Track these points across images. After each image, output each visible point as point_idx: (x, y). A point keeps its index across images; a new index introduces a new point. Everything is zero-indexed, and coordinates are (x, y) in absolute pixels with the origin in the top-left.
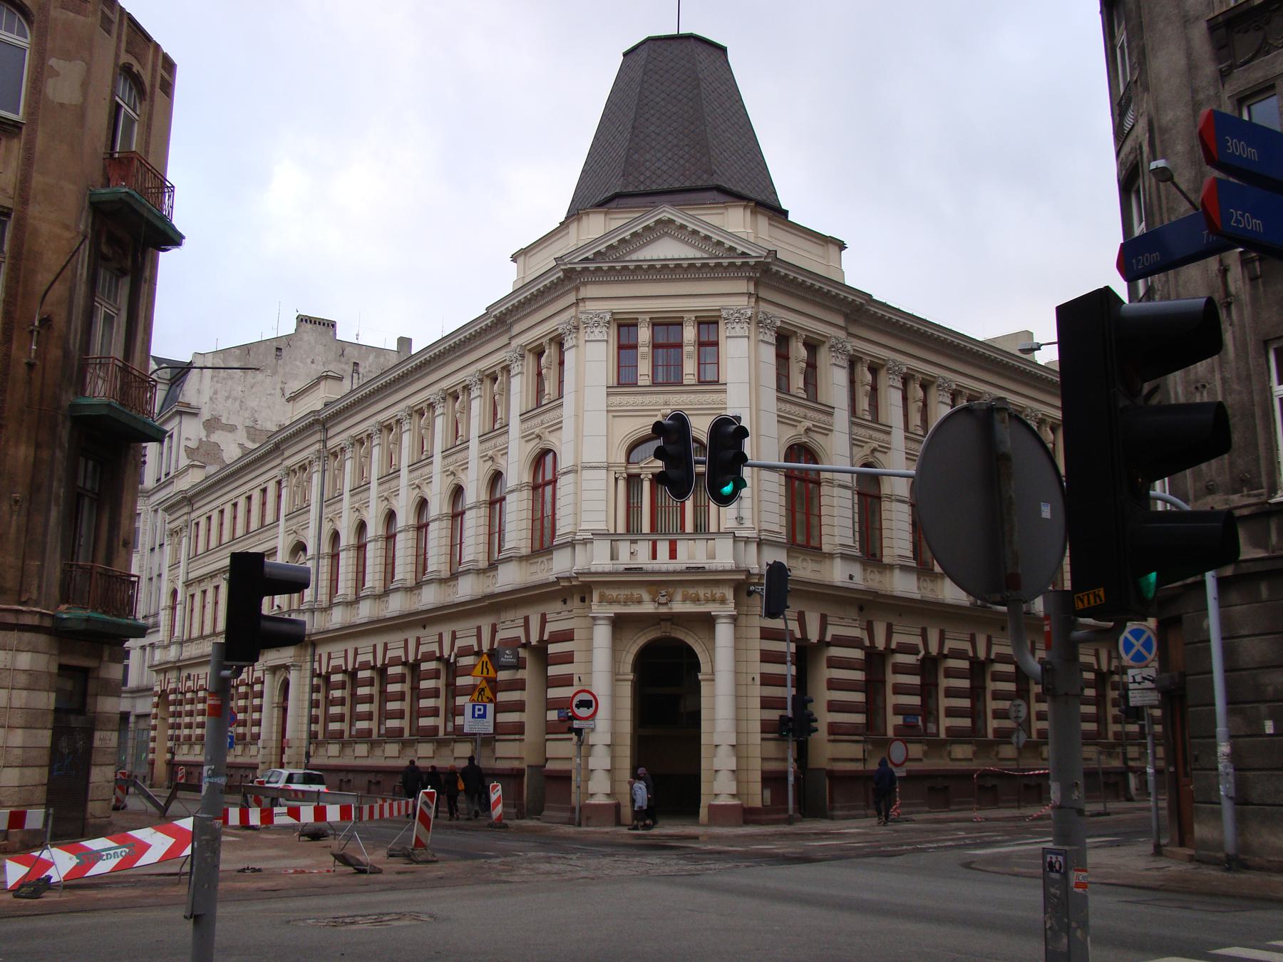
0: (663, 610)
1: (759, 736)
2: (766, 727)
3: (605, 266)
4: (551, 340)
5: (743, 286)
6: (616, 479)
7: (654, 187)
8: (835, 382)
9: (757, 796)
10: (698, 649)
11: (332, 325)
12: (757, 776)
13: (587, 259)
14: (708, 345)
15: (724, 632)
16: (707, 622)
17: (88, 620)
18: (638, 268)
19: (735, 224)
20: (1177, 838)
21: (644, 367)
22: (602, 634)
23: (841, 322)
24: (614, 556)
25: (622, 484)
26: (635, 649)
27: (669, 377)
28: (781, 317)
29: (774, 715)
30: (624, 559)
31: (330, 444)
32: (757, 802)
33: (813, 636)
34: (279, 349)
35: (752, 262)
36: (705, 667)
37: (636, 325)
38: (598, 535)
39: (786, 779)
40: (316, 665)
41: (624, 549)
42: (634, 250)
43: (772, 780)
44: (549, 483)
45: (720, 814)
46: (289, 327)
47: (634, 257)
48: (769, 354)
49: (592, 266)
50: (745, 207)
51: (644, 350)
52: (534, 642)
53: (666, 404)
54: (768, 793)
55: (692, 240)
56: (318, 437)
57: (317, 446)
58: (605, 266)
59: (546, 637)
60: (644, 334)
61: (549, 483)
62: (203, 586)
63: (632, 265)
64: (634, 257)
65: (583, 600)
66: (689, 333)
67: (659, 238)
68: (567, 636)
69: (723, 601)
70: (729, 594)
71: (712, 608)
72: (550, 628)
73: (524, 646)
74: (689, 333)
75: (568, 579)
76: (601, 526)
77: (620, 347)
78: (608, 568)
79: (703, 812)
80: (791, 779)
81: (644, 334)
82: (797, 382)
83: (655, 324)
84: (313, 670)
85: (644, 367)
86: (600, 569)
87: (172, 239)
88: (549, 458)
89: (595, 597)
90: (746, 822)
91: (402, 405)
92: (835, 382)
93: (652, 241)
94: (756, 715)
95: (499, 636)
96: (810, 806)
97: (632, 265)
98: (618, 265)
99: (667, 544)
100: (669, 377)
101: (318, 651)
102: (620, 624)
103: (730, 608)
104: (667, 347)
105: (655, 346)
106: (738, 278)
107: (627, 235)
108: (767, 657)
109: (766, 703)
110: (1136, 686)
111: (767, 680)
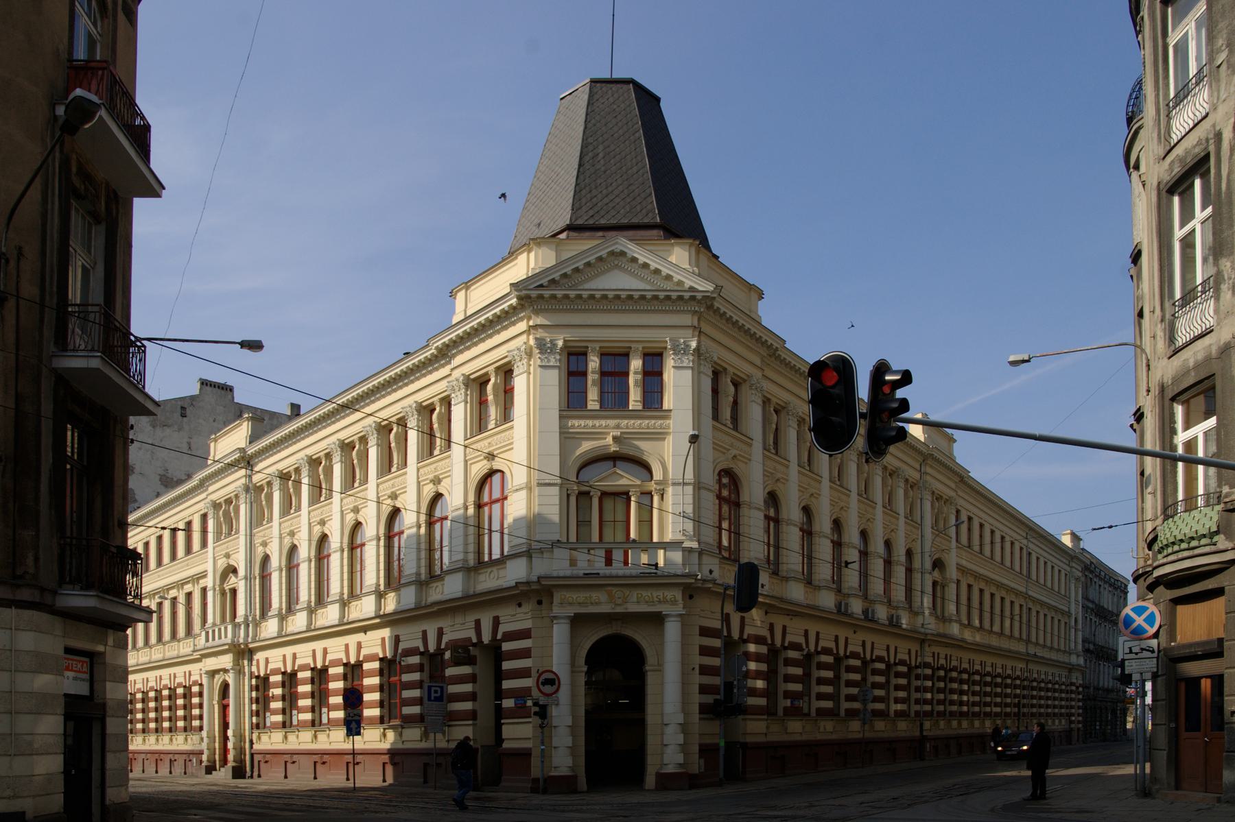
0: (619, 610)
1: (697, 716)
2: (704, 709)
3: (559, 293)
4: (498, 369)
5: (687, 319)
6: (568, 495)
7: (603, 222)
8: (754, 414)
9: (696, 766)
10: (644, 644)
11: (231, 389)
12: (696, 748)
13: (541, 286)
14: (653, 374)
15: (672, 630)
16: (656, 620)
17: (495, 396)
18: (592, 297)
19: (677, 260)
20: (1173, 784)
21: (593, 395)
22: (560, 632)
23: (758, 361)
24: (573, 563)
25: (573, 500)
26: (587, 645)
27: (615, 401)
28: (718, 353)
29: (709, 699)
30: (583, 566)
31: (256, 478)
32: (695, 769)
33: (736, 635)
34: (183, 408)
35: (699, 296)
36: (651, 659)
37: (585, 354)
38: (556, 544)
39: (718, 750)
40: (254, 669)
41: (582, 557)
42: (587, 281)
43: (707, 751)
44: (497, 501)
45: (666, 781)
46: (195, 390)
47: (587, 286)
48: (707, 384)
49: (547, 293)
50: (691, 245)
51: (592, 377)
52: (486, 639)
53: (618, 427)
54: (702, 761)
55: (644, 273)
56: (243, 472)
57: (243, 481)
58: (559, 293)
59: (499, 637)
60: (594, 363)
61: (497, 501)
62: (188, 588)
63: (585, 294)
64: (587, 286)
65: (540, 603)
66: (636, 364)
67: (608, 271)
68: (524, 634)
69: (674, 602)
70: (678, 594)
71: (665, 609)
72: (503, 629)
73: (474, 645)
74: (636, 364)
75: (528, 583)
76: (556, 537)
77: (570, 374)
78: (568, 573)
79: (650, 781)
80: (722, 752)
81: (594, 363)
82: (726, 413)
83: (603, 355)
84: (251, 673)
85: (593, 395)
86: (562, 574)
87: (153, 189)
88: (496, 479)
89: (556, 600)
90: (691, 787)
91: (334, 439)
92: (754, 414)
93: (603, 273)
94: (696, 699)
95: (445, 639)
96: (733, 775)
97: (585, 294)
98: (572, 294)
99: (621, 552)
100: (615, 401)
101: (255, 657)
102: (578, 621)
103: (679, 609)
104: (614, 373)
105: (603, 374)
106: (683, 312)
107: (592, 259)
108: (705, 651)
109: (704, 689)
110: (1133, 656)
111: (704, 670)
